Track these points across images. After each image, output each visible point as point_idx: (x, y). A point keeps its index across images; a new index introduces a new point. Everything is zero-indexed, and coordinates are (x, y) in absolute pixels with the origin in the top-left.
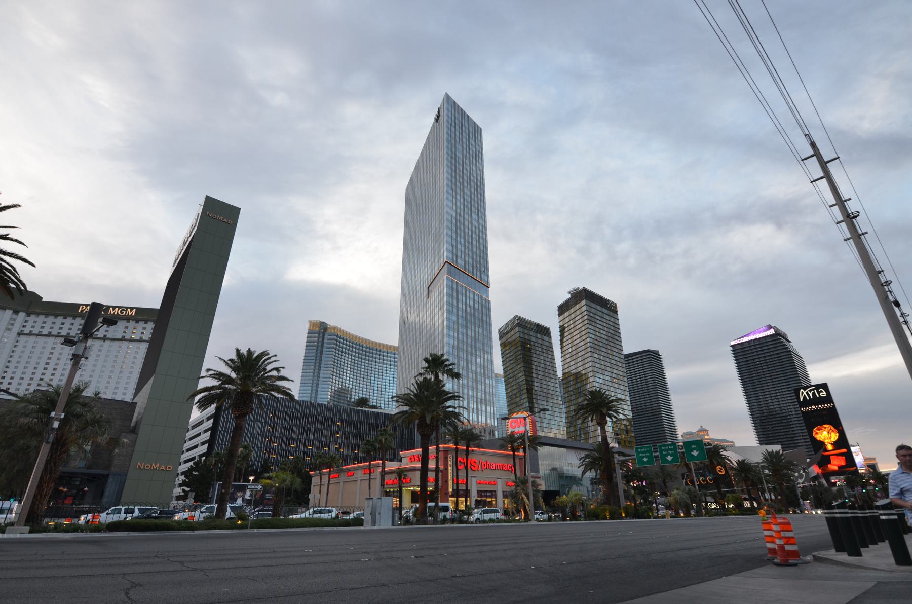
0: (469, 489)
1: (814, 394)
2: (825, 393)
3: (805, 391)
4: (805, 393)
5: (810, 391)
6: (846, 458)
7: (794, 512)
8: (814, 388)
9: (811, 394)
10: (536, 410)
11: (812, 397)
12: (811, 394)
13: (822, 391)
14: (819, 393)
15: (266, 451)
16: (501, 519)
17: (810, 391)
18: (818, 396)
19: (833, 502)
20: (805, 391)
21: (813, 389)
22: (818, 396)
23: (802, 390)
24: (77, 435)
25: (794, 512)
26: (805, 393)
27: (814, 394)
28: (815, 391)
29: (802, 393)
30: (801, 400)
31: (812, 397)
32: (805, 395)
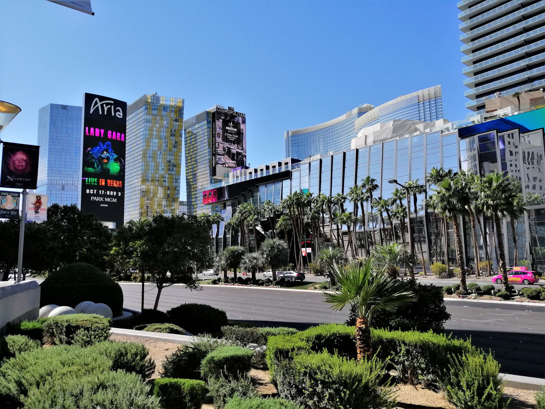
2: (121, 114)
3: (100, 102)
4: (99, 104)
8: (112, 102)
9: (106, 109)
11: (106, 113)
12: (106, 109)
13: (119, 111)
14: (116, 111)
17: (107, 104)
22: (113, 114)
23: (97, 99)
26: (99, 104)
28: (113, 107)
29: (96, 103)
30: (91, 112)
31: (106, 113)
32: (98, 107)
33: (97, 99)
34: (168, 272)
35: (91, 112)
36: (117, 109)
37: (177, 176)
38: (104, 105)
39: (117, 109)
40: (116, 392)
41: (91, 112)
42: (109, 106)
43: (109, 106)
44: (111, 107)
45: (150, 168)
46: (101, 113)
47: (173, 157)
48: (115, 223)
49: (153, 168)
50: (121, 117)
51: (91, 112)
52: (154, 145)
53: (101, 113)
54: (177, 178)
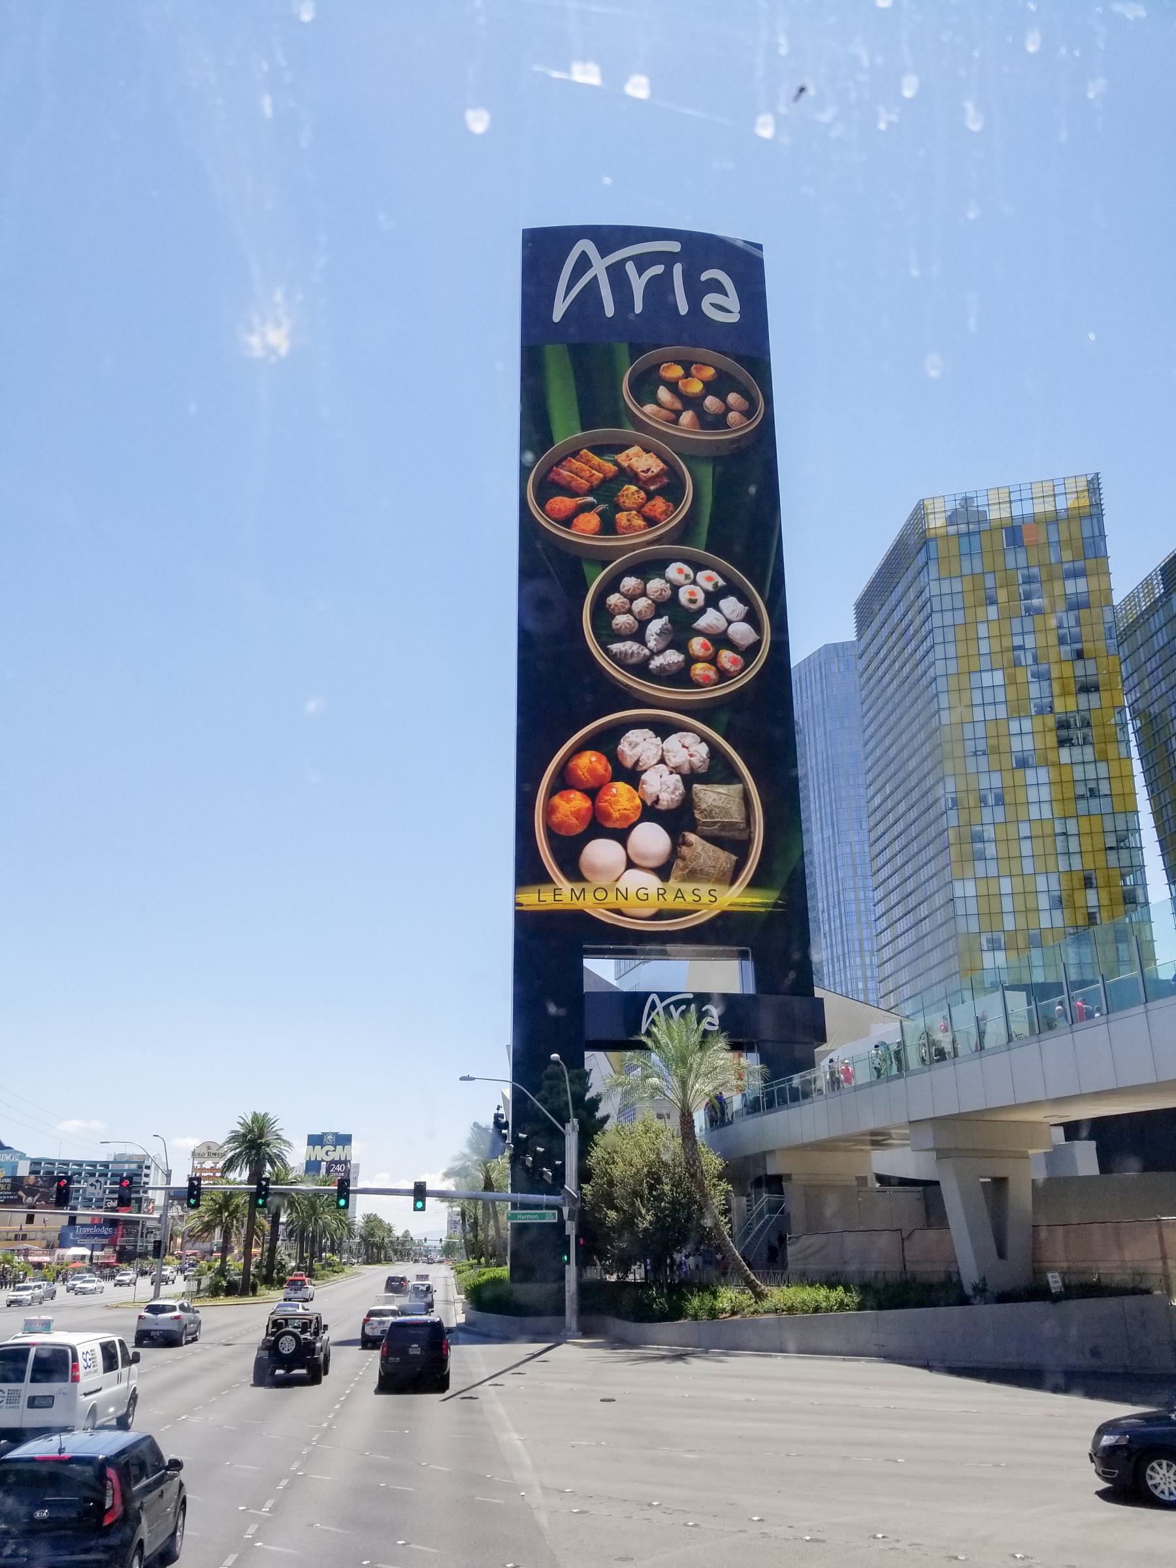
0: (1121, 1370)
1: (659, 289)
2: (732, 301)
3: (604, 253)
4: (599, 267)
5: (642, 263)
6: (1050, 1291)
7: (147, 1176)
8: (674, 247)
9: (638, 284)
10: (634, 1170)
11: (638, 308)
12: (638, 284)
13: (717, 287)
14: (696, 292)
15: (306, 1252)
16: (1003, 1369)
17: (642, 263)
18: (683, 308)
19: (565, 1099)
20: (604, 253)
21: (668, 259)
22: (683, 308)
23: (585, 246)
24: (703, 1315)
25: (147, 1176)
26: (599, 267)
28: (678, 269)
29: (584, 263)
30: (559, 311)
31: (638, 308)
32: (594, 282)
33: (585, 246)
34: (470, 115)
35: (557, 316)
36: (705, 276)
37: (1120, 820)
38: (630, 268)
39: (705, 276)
40: (53, 1247)
41: (557, 316)
42: (658, 269)
43: (658, 269)
44: (668, 274)
45: (960, 910)
46: (610, 310)
47: (1102, 769)
48: (749, 965)
49: (972, 909)
50: (734, 318)
51: (559, 311)
52: (989, 698)
53: (610, 310)
54: (1121, 826)
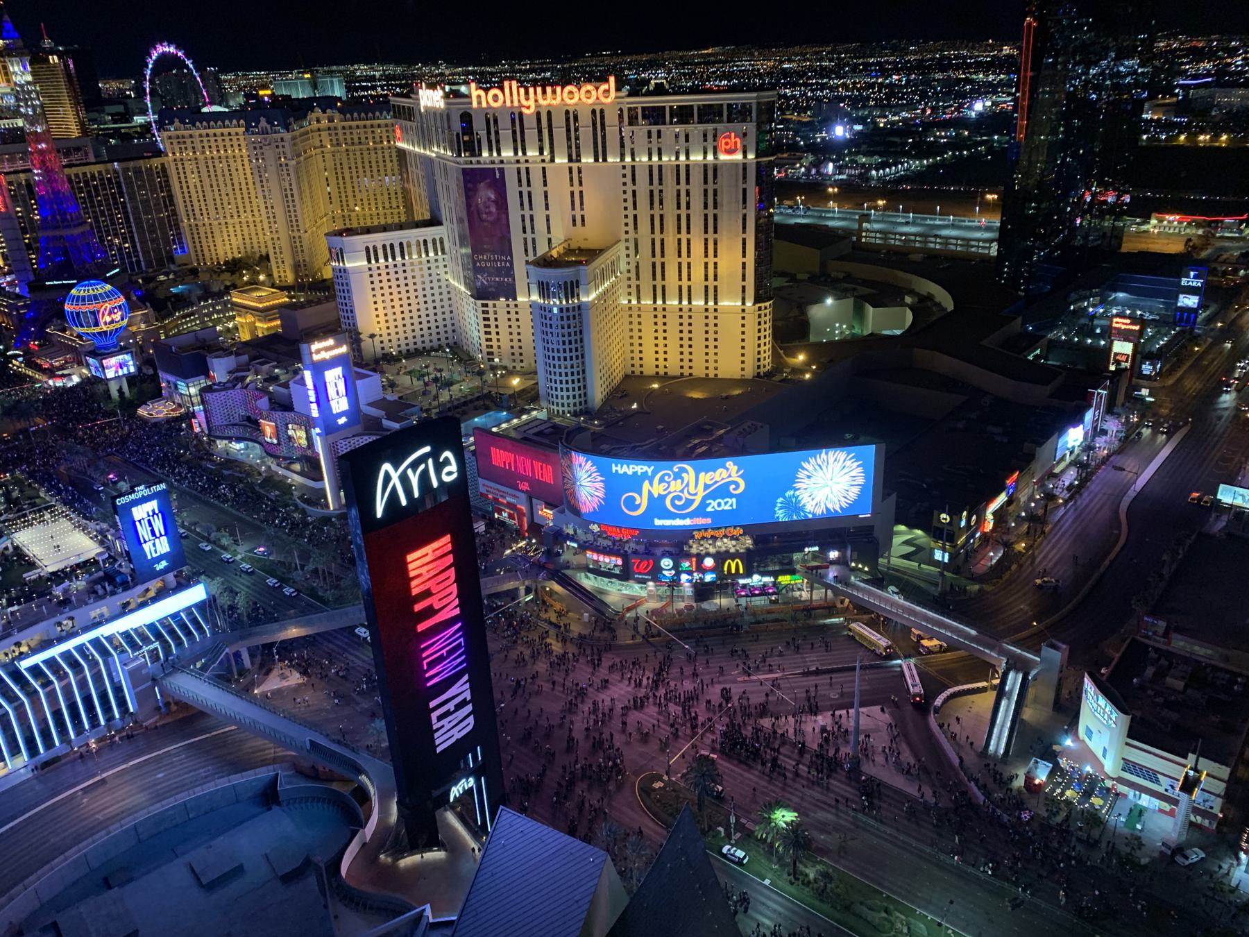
1: (424, 477)
12: (414, 480)
14: (439, 467)
27: (424, 477)
28: (430, 461)
29: (387, 478)
38: (410, 472)
46: (404, 502)
